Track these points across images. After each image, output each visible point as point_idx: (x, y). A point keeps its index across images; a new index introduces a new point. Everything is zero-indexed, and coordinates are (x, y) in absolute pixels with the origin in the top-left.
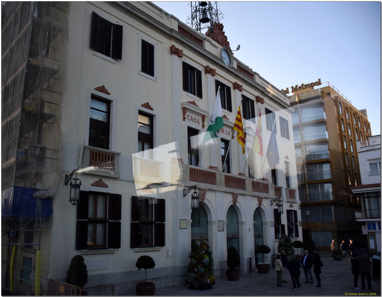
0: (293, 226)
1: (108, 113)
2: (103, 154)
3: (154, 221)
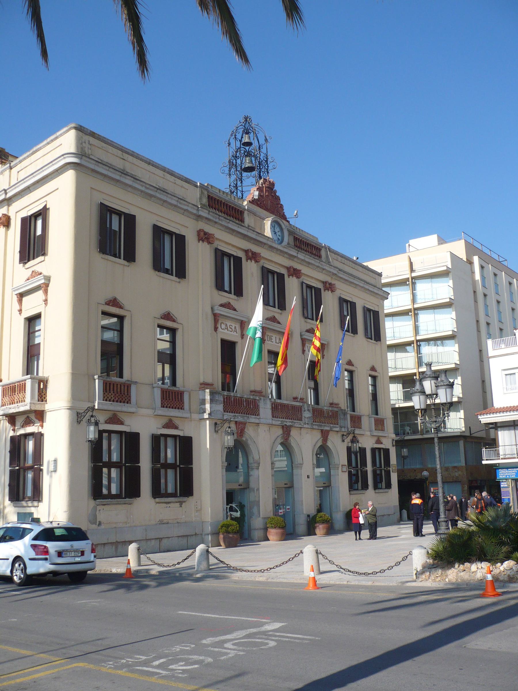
0: (381, 472)
1: (173, 342)
2: (114, 384)
3: (178, 464)
